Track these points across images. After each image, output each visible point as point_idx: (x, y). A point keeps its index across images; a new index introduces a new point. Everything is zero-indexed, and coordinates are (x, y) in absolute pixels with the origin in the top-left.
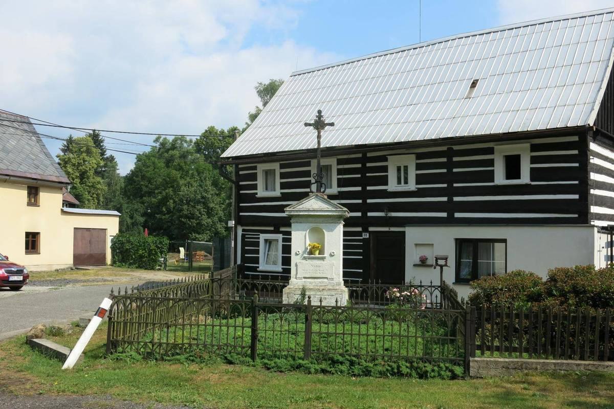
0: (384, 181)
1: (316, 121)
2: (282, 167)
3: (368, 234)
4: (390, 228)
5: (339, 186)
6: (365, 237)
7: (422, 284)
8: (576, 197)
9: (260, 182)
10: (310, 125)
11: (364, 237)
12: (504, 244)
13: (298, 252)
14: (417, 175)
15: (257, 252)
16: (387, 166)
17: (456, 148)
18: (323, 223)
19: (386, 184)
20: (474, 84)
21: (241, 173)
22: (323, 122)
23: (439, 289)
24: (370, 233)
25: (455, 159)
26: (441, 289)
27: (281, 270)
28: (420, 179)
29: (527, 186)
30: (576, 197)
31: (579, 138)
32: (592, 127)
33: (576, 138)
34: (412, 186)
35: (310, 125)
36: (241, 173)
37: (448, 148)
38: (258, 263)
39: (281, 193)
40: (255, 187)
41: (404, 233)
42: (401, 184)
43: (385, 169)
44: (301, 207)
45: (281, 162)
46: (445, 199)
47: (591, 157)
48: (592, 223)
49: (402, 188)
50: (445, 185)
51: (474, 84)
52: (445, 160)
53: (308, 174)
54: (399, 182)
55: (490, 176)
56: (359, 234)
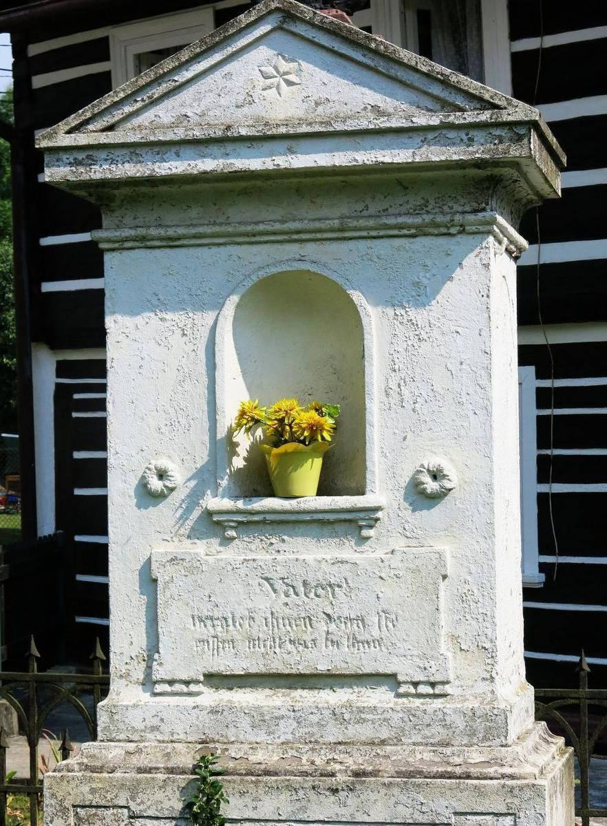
18: (342, 234)
44: (164, 113)
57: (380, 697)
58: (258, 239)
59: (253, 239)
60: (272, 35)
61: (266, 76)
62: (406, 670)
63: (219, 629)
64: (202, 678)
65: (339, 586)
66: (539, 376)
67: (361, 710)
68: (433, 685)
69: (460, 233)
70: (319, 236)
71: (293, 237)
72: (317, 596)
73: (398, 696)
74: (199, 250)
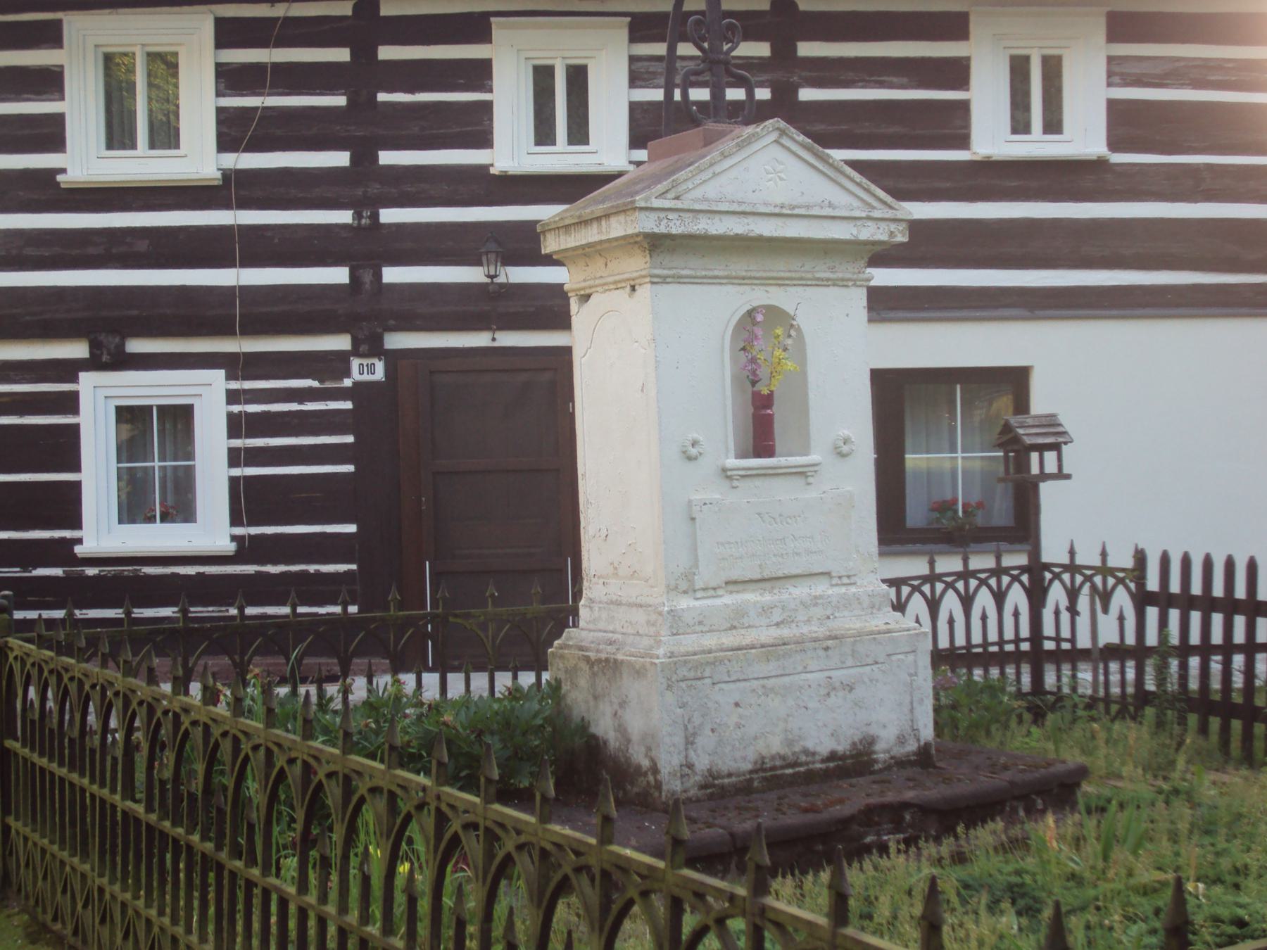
2: (228, 34)
3: (380, 367)
4: (498, 335)
5: (226, 143)
6: (367, 377)
11: (356, 376)
16: (968, 59)
18: (803, 282)
19: (483, 140)
24: (394, 359)
25: (807, 49)
26: (1030, 579)
27: (229, 547)
29: (1099, 165)
38: (76, 523)
42: (553, 143)
43: (479, 74)
44: (711, 190)
46: (338, 275)
52: (341, 55)
54: (544, 134)
56: (334, 364)
57: (821, 588)
58: (745, 281)
59: (743, 282)
60: (771, 146)
61: (768, 173)
62: (836, 569)
63: (734, 550)
64: (724, 585)
65: (799, 516)
66: (229, 377)
67: (816, 597)
68: (849, 577)
69: (853, 285)
70: (780, 282)
71: (765, 281)
72: (788, 523)
73: (697, 599)
74: (695, 286)
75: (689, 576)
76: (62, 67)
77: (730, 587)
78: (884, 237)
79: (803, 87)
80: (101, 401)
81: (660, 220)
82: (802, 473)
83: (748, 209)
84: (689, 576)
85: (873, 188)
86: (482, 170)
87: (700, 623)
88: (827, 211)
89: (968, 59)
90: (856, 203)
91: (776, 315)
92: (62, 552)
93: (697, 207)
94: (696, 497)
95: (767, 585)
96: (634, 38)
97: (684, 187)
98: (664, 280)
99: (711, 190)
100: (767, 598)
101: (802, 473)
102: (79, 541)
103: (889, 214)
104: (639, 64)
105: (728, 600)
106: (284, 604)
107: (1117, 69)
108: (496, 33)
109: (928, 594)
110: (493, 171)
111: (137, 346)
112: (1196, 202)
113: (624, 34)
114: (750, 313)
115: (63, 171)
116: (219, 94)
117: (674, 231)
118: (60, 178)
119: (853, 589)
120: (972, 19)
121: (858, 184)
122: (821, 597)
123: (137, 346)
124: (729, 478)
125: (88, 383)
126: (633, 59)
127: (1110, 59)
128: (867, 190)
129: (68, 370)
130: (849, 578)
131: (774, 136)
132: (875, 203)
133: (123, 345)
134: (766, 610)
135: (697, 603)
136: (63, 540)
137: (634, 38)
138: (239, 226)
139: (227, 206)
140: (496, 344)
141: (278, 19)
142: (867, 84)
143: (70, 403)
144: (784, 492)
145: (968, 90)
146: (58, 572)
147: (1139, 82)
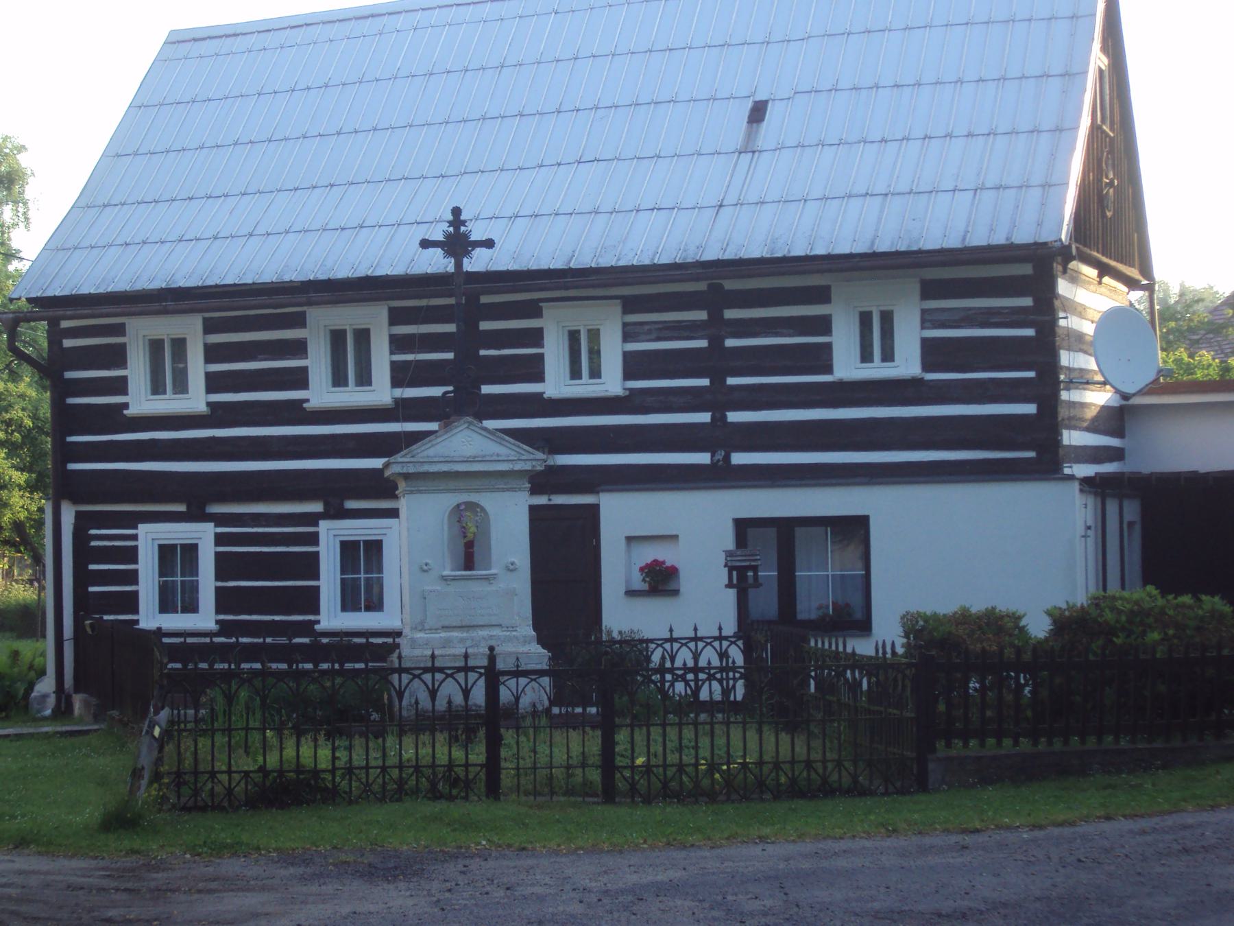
0: (534, 369)
1: (448, 236)
2: (210, 327)
4: (553, 497)
5: (396, 382)
7: (699, 635)
8: (1030, 409)
9: (137, 370)
10: (434, 244)
12: (799, 532)
13: (426, 565)
14: (626, 355)
15: (132, 577)
16: (830, 315)
17: (729, 285)
19: (539, 377)
20: (758, 113)
21: (68, 343)
22: (466, 236)
23: (740, 643)
25: (730, 314)
28: (634, 366)
29: (915, 382)
30: (1030, 409)
31: (1034, 267)
32: (1069, 246)
33: (1027, 269)
34: (612, 383)
35: (434, 244)
36: (68, 343)
37: (709, 286)
38: (136, 611)
39: (208, 404)
40: (120, 386)
41: (595, 508)
42: (580, 378)
43: (536, 337)
44: (431, 452)
45: (208, 315)
46: (705, 417)
47: (1061, 314)
48: (1067, 471)
49: (585, 388)
50: (705, 382)
51: (758, 113)
53: (299, 348)
54: (575, 374)
55: (821, 358)
71: (469, 491)
75: (422, 623)
76: (306, 339)
77: (445, 629)
78: (530, 468)
79: (727, 338)
80: (331, 538)
81: (403, 467)
82: (487, 578)
83: (449, 459)
84: (422, 623)
85: (521, 445)
86: (539, 396)
87: (427, 644)
88: (495, 458)
89: (830, 315)
90: (513, 453)
91: (472, 507)
92: (307, 628)
93: (421, 460)
94: (427, 588)
95: (466, 629)
96: (626, 311)
97: (415, 452)
98: (412, 492)
99: (431, 452)
100: (465, 635)
101: (487, 578)
102: (318, 622)
103: (532, 457)
104: (628, 327)
105: (443, 635)
106: (260, 638)
107: (927, 317)
108: (545, 312)
109: (693, 649)
110: (545, 396)
111: (351, 504)
112: (984, 404)
113: (619, 309)
114: (458, 506)
115: (307, 401)
116: (392, 353)
117: (410, 472)
118: (305, 405)
119: (514, 633)
120: (833, 290)
121: (514, 444)
122: (494, 636)
123: (351, 504)
124: (446, 580)
125: (324, 526)
126: (625, 325)
127: (923, 312)
128: (519, 447)
129: (312, 519)
130: (513, 628)
131: (466, 425)
132: (523, 452)
133: (343, 505)
134: (462, 640)
135: (426, 636)
136: (310, 621)
137: (626, 311)
138: (404, 432)
139: (397, 420)
140: (552, 503)
141: (423, 307)
142: (767, 335)
143: (313, 539)
144: (476, 587)
145: (831, 335)
146: (306, 640)
147: (943, 325)
